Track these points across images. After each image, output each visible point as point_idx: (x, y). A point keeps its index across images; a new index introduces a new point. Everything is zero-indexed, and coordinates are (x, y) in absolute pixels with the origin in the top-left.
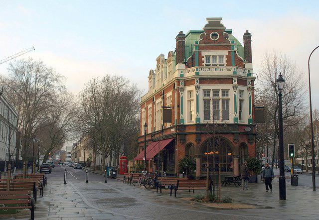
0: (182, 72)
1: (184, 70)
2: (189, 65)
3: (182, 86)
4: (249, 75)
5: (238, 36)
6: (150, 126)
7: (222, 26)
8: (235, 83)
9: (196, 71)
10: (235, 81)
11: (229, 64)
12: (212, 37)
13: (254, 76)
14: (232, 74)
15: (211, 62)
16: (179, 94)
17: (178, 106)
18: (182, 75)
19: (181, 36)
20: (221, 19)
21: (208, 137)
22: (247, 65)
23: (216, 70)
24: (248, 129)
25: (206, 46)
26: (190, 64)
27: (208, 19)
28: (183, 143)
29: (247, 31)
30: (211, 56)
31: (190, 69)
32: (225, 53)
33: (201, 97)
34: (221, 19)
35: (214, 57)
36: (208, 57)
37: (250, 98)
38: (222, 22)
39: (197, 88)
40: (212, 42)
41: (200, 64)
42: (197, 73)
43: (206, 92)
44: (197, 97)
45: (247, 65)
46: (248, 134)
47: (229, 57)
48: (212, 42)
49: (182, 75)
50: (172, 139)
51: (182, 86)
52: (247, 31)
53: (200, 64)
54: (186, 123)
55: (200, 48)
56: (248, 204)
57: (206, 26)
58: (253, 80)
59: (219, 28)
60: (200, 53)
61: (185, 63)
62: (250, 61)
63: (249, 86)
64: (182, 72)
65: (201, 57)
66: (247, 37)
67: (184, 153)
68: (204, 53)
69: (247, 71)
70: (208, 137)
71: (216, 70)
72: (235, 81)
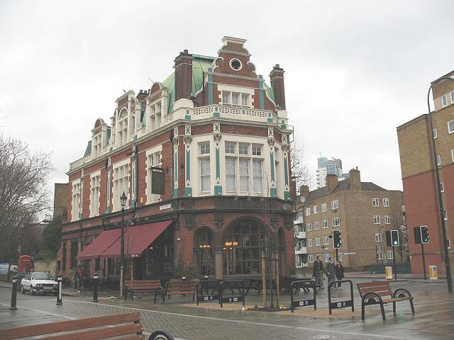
0: (188, 112)
1: (191, 109)
2: (200, 101)
3: (188, 134)
4: (284, 127)
5: (263, 70)
6: (94, 198)
7: (246, 51)
8: (216, 132)
9: (268, 117)
10: (188, 130)
11: (256, 105)
12: (233, 65)
13: (291, 128)
14: (212, 116)
15: (240, 104)
16: (182, 149)
17: (182, 167)
18: (188, 117)
19: (185, 57)
20: (244, 41)
21: (234, 217)
22: (280, 113)
23: (244, 113)
24: (285, 207)
25: (223, 78)
26: (200, 101)
27: (226, 38)
28: (190, 228)
29: (277, 67)
30: (241, 95)
31: (203, 108)
32: (251, 92)
33: (223, 154)
34: (244, 41)
35: (236, 95)
36: (226, 94)
37: (285, 160)
38: (245, 46)
39: (217, 138)
40: (232, 72)
41: (216, 101)
42: (217, 115)
43: (230, 146)
44: (217, 151)
45: (280, 113)
46: (185, 213)
47: (256, 97)
48: (232, 72)
49: (188, 117)
50: (171, 222)
51: (188, 134)
52: (277, 67)
53: (216, 101)
54: (195, 194)
55: (216, 79)
56: (425, 317)
57: (224, 47)
58: (288, 134)
59: (243, 54)
60: (215, 87)
61: (192, 99)
62: (283, 107)
63: (285, 143)
64: (188, 112)
65: (217, 93)
66: (277, 74)
67: (192, 245)
68: (221, 88)
69: (280, 121)
70: (234, 217)
71: (244, 113)
72: (188, 130)
